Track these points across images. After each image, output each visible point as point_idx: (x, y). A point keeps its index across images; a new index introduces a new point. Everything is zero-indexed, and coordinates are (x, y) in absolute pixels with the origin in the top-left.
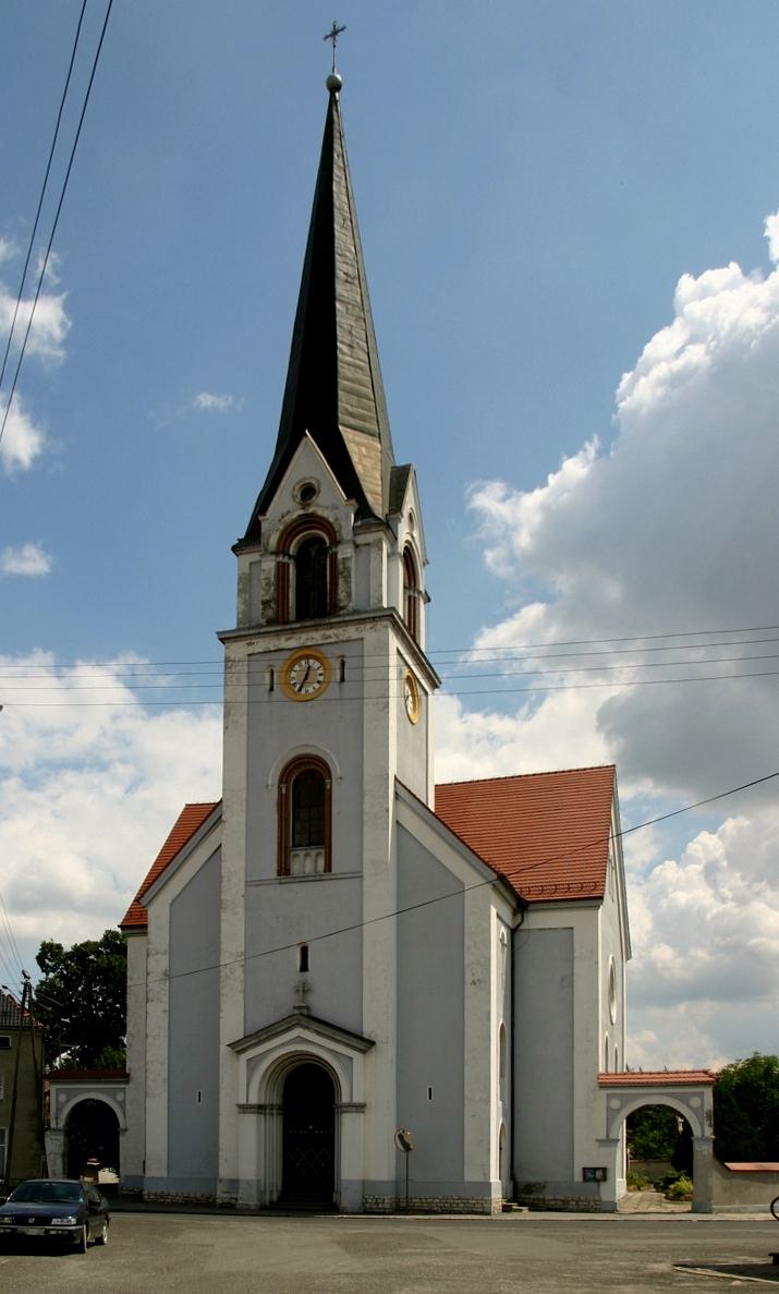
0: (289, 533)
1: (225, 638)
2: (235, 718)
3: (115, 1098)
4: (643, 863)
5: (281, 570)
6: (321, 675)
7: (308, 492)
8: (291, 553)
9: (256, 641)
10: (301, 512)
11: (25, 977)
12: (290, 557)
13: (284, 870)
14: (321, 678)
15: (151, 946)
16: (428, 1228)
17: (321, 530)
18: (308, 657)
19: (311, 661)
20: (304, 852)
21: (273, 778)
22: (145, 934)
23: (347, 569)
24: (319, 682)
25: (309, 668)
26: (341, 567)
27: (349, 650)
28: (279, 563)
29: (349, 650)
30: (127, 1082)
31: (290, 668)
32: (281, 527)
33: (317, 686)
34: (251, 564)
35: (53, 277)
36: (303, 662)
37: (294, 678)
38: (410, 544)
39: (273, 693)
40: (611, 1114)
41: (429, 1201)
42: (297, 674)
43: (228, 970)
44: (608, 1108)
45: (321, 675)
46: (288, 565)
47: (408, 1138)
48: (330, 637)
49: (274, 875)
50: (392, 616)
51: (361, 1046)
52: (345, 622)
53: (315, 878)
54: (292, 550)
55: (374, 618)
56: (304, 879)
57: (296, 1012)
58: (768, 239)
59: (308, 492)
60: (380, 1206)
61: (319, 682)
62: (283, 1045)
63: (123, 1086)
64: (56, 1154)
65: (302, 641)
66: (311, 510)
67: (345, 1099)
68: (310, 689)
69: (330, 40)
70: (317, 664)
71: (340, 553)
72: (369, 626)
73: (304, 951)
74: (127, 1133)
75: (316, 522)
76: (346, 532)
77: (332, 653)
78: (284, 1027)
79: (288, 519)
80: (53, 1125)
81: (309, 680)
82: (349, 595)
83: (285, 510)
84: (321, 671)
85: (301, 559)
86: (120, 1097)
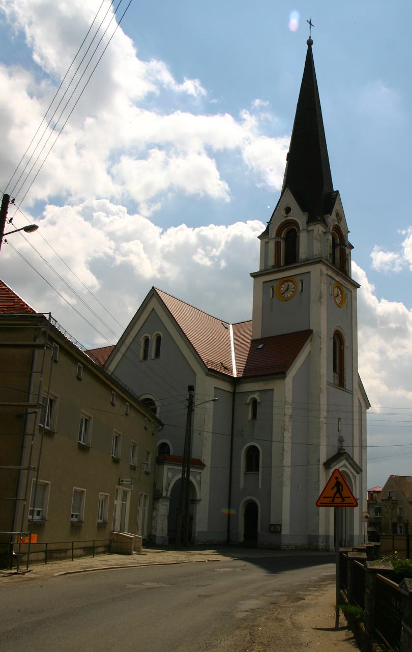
1: (254, 275)
3: (195, 478)
4: (239, 120)
8: (282, 237)
14: (293, 290)
16: (280, 223)
18: (287, 281)
19: (289, 283)
24: (292, 291)
25: (288, 286)
28: (276, 242)
30: (202, 469)
31: (280, 286)
33: (291, 293)
34: (266, 243)
36: (286, 283)
37: (282, 291)
39: (273, 299)
42: (283, 289)
46: (280, 242)
50: (321, 261)
54: (283, 236)
58: (287, 160)
61: (292, 291)
63: (200, 471)
64: (164, 515)
68: (289, 294)
69: (309, 20)
70: (292, 284)
74: (201, 503)
75: (291, 223)
77: (297, 279)
80: (164, 494)
81: (288, 291)
84: (293, 286)
85: (286, 239)
86: (198, 478)
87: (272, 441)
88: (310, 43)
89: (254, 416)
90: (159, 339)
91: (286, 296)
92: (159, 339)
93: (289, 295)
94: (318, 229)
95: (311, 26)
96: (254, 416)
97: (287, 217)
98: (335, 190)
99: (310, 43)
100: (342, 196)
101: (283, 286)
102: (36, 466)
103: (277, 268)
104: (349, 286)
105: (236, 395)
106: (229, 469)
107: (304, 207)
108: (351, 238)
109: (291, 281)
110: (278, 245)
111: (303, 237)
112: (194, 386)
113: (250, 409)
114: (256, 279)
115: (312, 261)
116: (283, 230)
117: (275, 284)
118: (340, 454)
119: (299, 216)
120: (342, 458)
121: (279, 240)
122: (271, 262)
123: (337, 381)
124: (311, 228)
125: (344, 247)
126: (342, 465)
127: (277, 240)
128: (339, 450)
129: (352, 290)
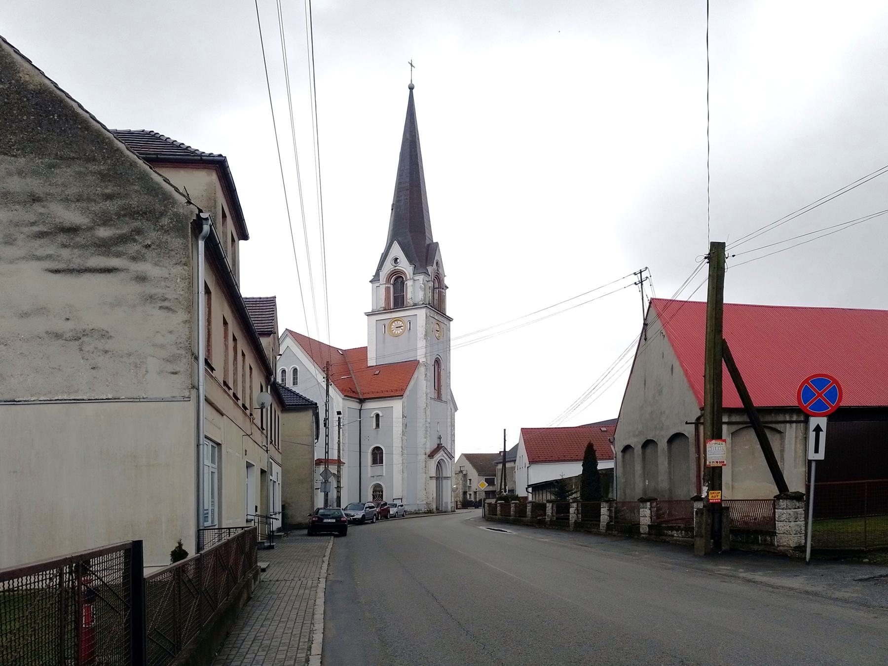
1: (368, 315)
8: (391, 283)
87: (393, 454)
88: (411, 88)
89: (378, 425)
90: (295, 371)
91: (396, 333)
92: (295, 371)
93: (399, 332)
94: (421, 278)
95: (413, 68)
96: (378, 425)
97: (396, 267)
98: (434, 241)
99: (411, 88)
100: (441, 247)
101: (394, 324)
102: (239, 645)
103: (387, 310)
104: (446, 321)
105: (361, 411)
106: (362, 465)
107: (410, 260)
108: (447, 281)
109: (401, 321)
110: (388, 289)
111: (409, 283)
112: (345, 537)
113: (374, 419)
114: (369, 317)
115: (415, 306)
116: (391, 279)
117: (387, 322)
118: (439, 447)
119: (405, 266)
120: (441, 450)
121: (389, 286)
122: (382, 304)
123: (435, 396)
124: (416, 278)
125: (441, 290)
126: (440, 455)
127: (387, 286)
128: (438, 445)
129: (447, 324)
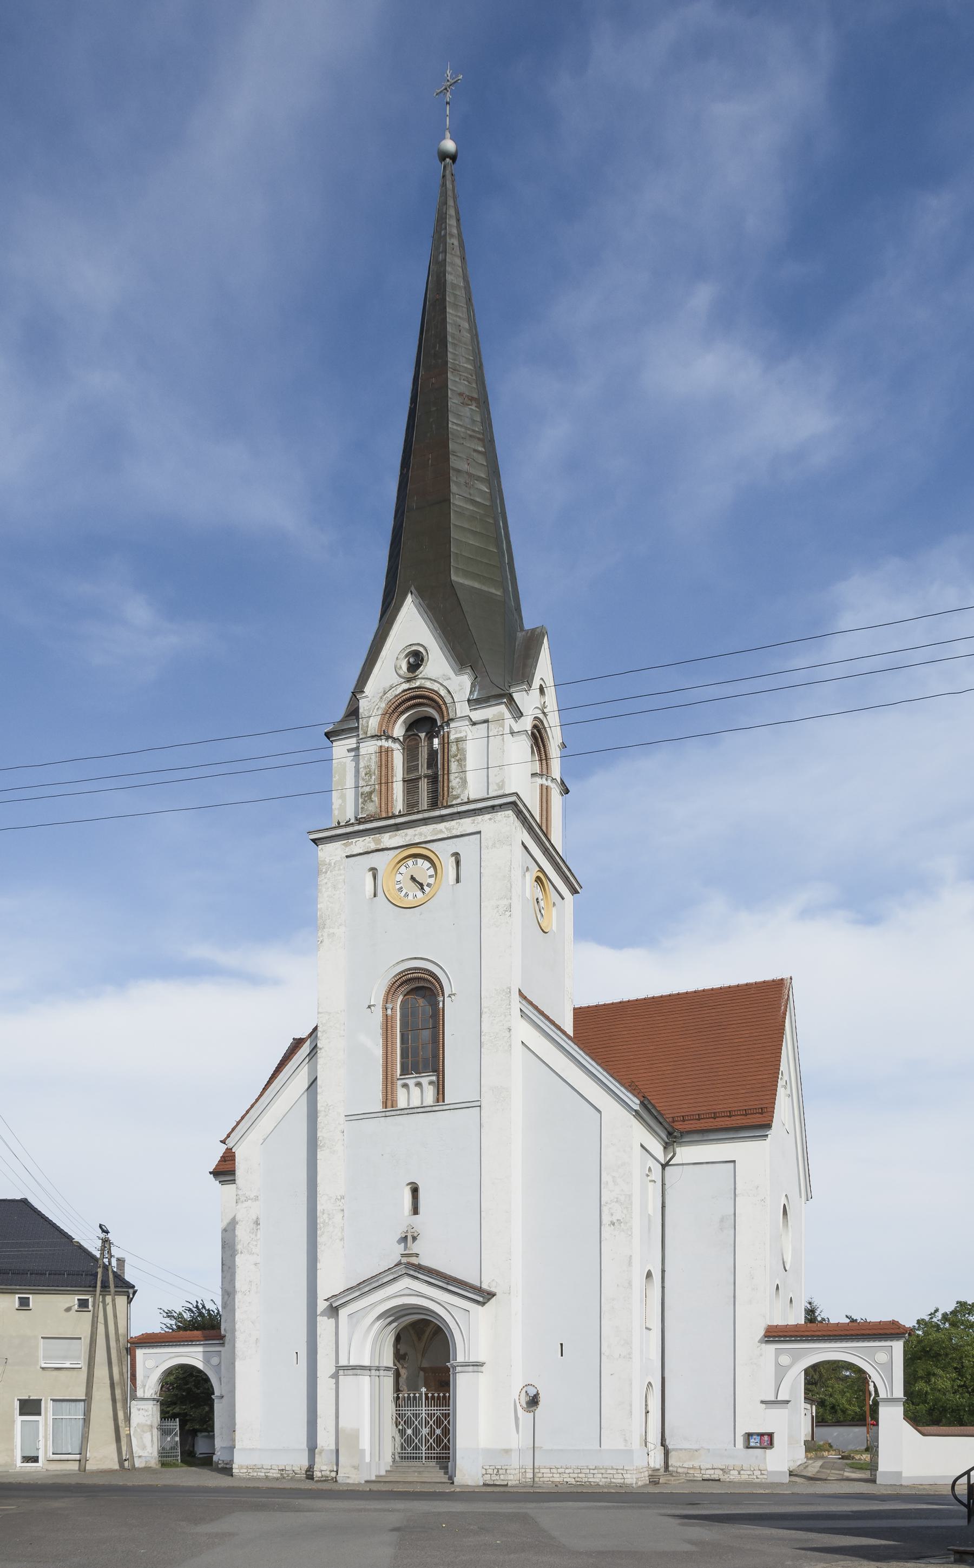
0: (395, 709)
2: (331, 931)
5: (385, 754)
6: (431, 876)
7: (416, 660)
9: (354, 840)
10: (406, 686)
11: (103, 1231)
12: (395, 740)
13: (389, 1101)
15: (240, 1192)
17: (433, 708)
20: (414, 1081)
21: (377, 995)
22: (233, 1181)
23: (461, 751)
26: (453, 749)
27: (465, 847)
29: (465, 847)
32: (383, 705)
35: (423, 738)
38: (542, 722)
40: (780, 1371)
41: (560, 1471)
43: (325, 1216)
44: (777, 1364)
45: (431, 876)
47: (528, 1392)
48: (441, 831)
49: (379, 1107)
51: (394, 1102)
52: (459, 813)
53: (423, 1109)
55: (493, 807)
56: (410, 1111)
57: (404, 1260)
59: (416, 660)
60: (502, 1477)
62: (389, 1298)
65: (408, 838)
66: (418, 683)
67: (460, 1358)
71: (453, 732)
72: (487, 816)
73: (415, 1191)
76: (462, 709)
77: (443, 852)
78: (391, 1277)
79: (390, 695)
82: (464, 782)
83: (387, 685)
